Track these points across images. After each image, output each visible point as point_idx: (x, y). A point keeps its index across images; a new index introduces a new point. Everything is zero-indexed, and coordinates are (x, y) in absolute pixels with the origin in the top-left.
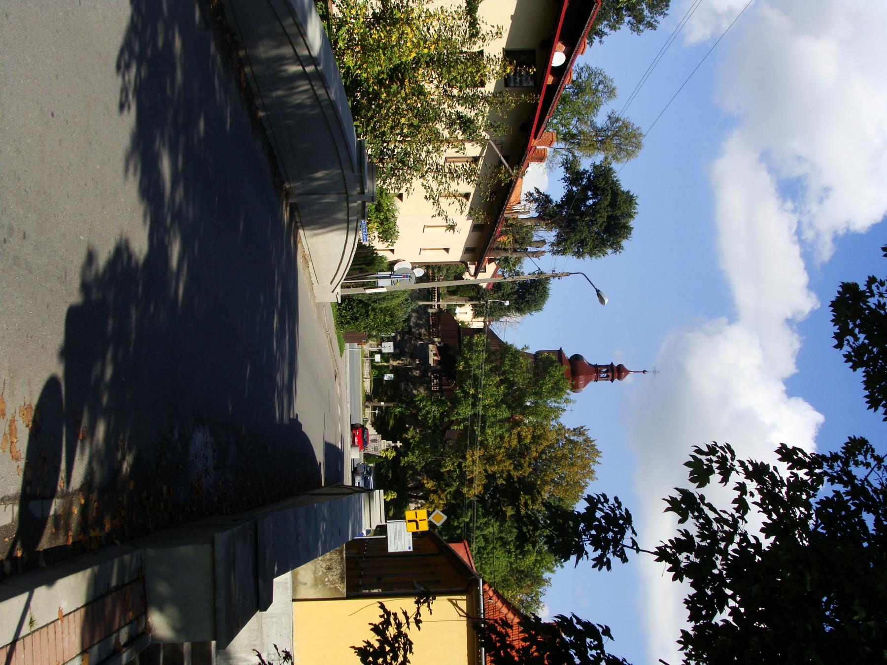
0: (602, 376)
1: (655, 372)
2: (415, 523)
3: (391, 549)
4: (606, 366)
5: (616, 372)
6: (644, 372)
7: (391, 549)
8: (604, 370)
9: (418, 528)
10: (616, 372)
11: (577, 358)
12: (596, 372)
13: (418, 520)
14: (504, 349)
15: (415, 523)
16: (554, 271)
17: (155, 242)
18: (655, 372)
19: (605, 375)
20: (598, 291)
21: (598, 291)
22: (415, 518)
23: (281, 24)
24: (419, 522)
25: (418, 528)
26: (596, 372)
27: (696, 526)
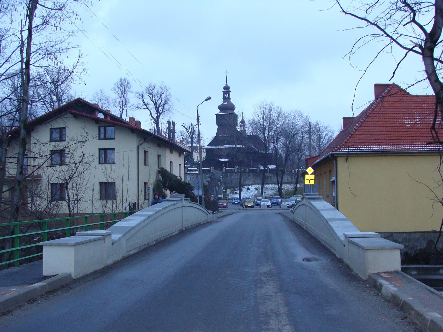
0: (228, 96)
1: (226, 73)
2: (311, 181)
3: (314, 184)
4: (224, 95)
5: (227, 90)
6: (226, 77)
7: (314, 184)
8: (225, 95)
9: (313, 180)
10: (227, 90)
11: (221, 108)
12: (227, 98)
13: (309, 179)
14: (215, 142)
15: (311, 181)
16: (196, 119)
17: (335, 168)
18: (226, 73)
19: (228, 95)
20: (205, 100)
21: (205, 100)
22: (309, 180)
23: (182, 225)
24: (310, 179)
25: (313, 180)
26: (227, 98)
27: (375, 296)
